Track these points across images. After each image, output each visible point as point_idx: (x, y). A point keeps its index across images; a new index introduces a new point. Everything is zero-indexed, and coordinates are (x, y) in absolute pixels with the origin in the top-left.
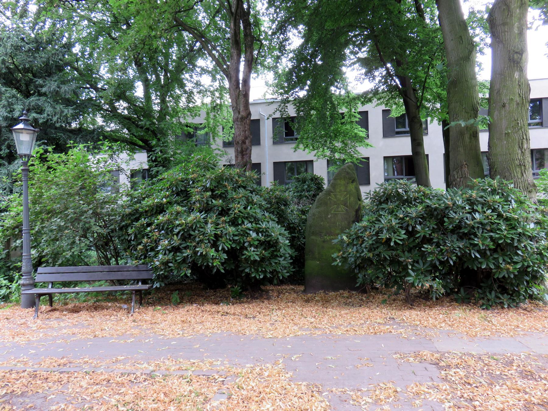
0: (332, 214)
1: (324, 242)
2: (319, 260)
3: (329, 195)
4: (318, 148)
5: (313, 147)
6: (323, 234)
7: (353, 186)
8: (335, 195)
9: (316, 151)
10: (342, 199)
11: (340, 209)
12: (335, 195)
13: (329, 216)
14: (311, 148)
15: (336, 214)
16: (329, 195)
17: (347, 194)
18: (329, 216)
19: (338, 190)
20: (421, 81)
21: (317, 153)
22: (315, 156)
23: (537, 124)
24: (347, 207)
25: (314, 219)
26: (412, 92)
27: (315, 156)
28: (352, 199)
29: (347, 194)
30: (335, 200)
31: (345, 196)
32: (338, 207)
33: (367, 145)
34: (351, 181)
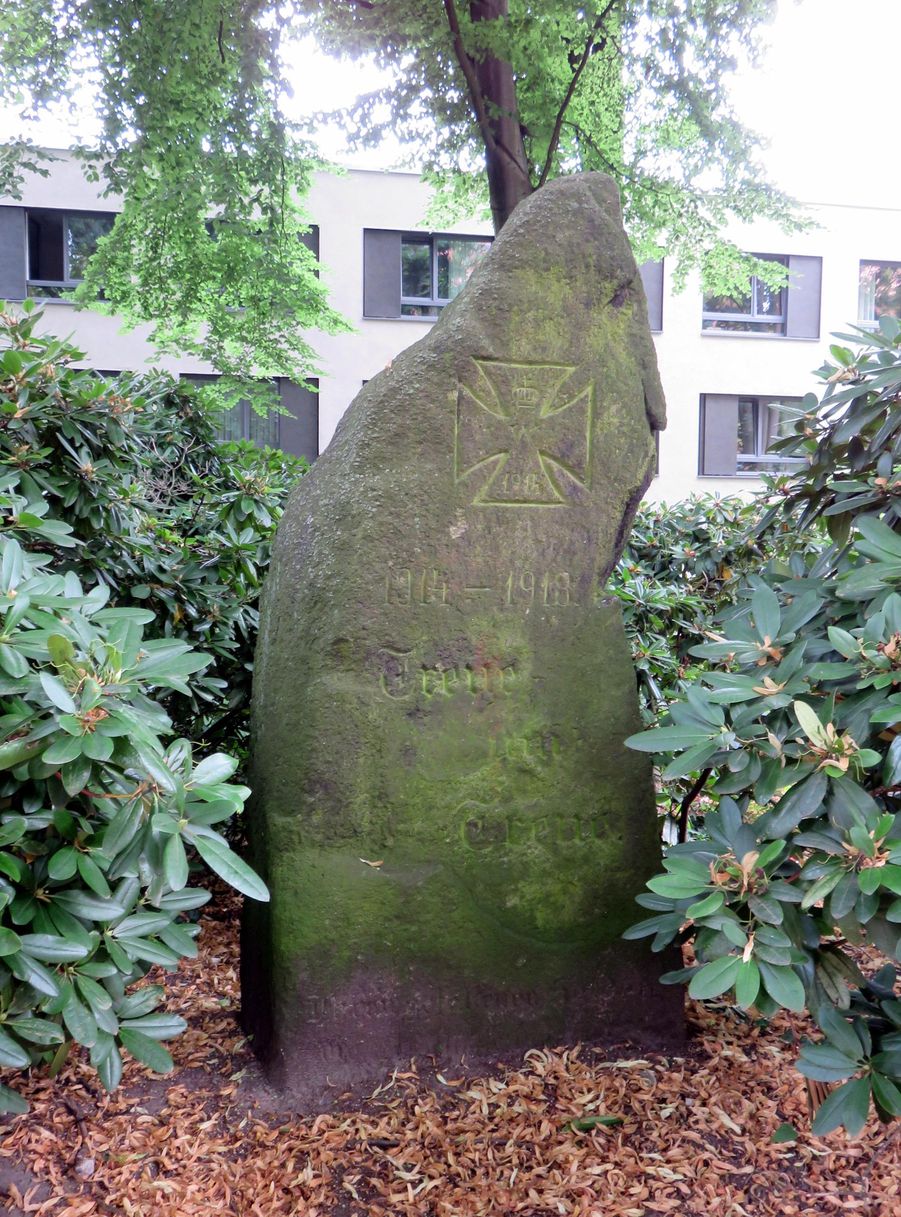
0: (471, 514)
1: (414, 713)
2: (380, 848)
3: (463, 374)
4: (163, 312)
5: (146, 308)
6: (408, 661)
7: (621, 329)
8: (503, 382)
9: (155, 323)
10: (545, 413)
11: (529, 484)
12: (503, 382)
13: (455, 532)
14: (138, 307)
15: (501, 518)
16: (463, 374)
17: (579, 381)
18: (455, 532)
19: (522, 347)
20: (549, 99)
21: (160, 329)
22: (152, 339)
23: (771, 327)
24: (576, 469)
25: (343, 548)
26: (517, 131)
27: (152, 339)
28: (613, 416)
29: (579, 381)
30: (501, 416)
31: (568, 391)
32: (515, 470)
33: (336, 322)
34: (609, 287)
